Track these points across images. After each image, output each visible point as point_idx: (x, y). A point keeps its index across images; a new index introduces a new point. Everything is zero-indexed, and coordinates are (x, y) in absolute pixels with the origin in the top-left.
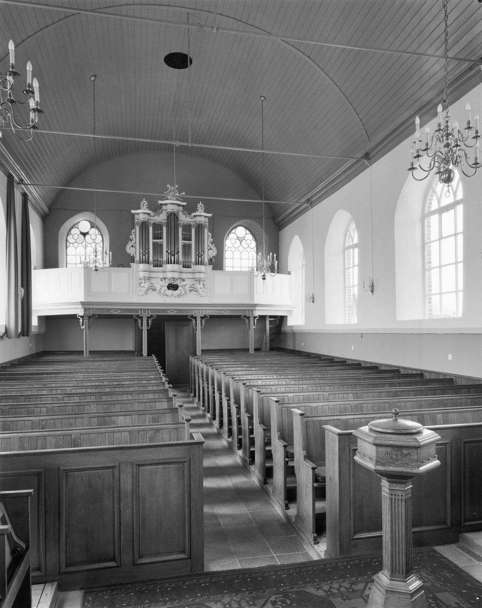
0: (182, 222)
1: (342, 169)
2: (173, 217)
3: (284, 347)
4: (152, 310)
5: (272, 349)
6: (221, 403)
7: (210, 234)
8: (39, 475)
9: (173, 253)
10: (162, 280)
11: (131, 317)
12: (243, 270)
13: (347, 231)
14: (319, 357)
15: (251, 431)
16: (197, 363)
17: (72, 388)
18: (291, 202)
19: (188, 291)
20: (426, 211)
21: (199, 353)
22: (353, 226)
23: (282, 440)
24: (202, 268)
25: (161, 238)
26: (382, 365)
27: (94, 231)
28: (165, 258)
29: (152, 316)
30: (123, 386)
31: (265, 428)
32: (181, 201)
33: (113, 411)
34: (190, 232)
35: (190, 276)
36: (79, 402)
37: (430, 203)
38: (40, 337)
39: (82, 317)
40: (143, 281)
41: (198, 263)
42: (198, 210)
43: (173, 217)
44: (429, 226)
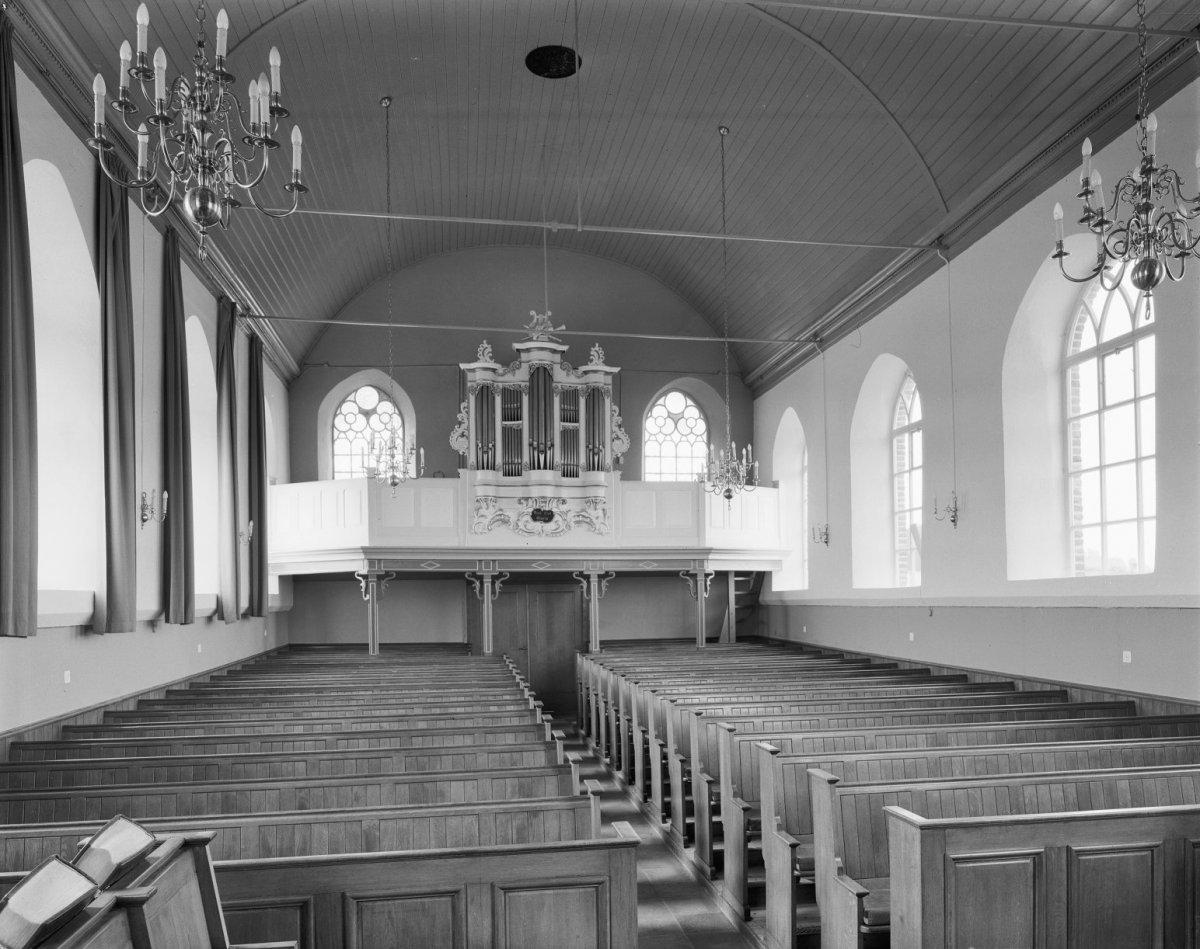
0: (559, 385)
1: (889, 269)
2: (541, 377)
3: (766, 635)
4: (501, 562)
5: (740, 639)
6: (646, 751)
7: (616, 408)
8: (304, 907)
9: (542, 447)
10: (520, 503)
11: (459, 576)
12: (681, 479)
13: (897, 398)
14: (838, 655)
15: (716, 810)
16: (592, 670)
17: (352, 720)
18: (779, 340)
19: (572, 524)
20: (1070, 352)
21: (594, 647)
22: (911, 385)
23: (784, 832)
24: (600, 476)
25: (519, 418)
26: (976, 672)
27: (387, 407)
28: (526, 459)
29: (501, 574)
30: (453, 717)
31: (746, 805)
32: (557, 342)
33: (438, 769)
34: (577, 404)
35: (577, 493)
36: (368, 751)
37: (1078, 337)
38: (284, 617)
39: (365, 577)
40: (484, 505)
41: (592, 466)
42: (592, 361)
43: (541, 377)
44: (1076, 384)
